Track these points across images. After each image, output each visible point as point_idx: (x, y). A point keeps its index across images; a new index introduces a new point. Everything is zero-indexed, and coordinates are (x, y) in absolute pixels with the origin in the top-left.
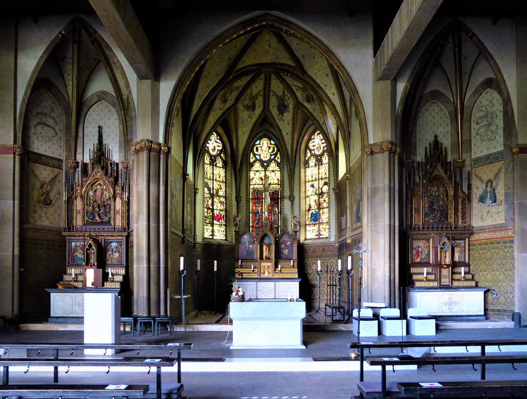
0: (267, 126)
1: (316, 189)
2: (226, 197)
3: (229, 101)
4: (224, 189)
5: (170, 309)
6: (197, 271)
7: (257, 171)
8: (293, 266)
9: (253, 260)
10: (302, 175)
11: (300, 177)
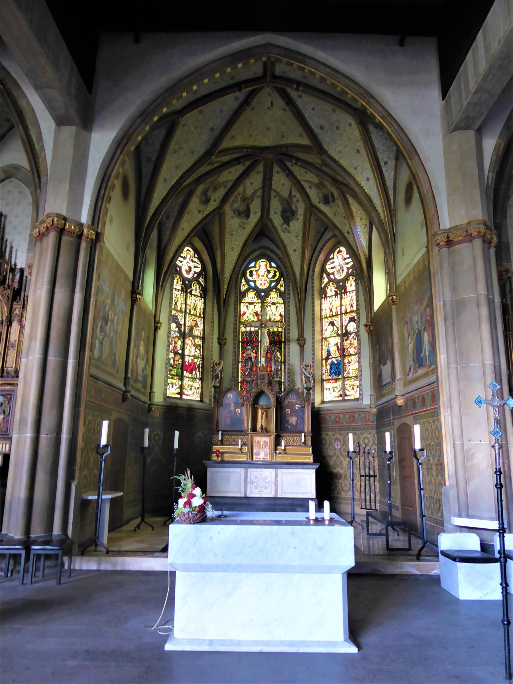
0: (265, 242)
1: (338, 328)
2: (203, 339)
3: (212, 202)
4: (201, 327)
5: (73, 522)
6: (143, 449)
7: (251, 303)
8: (305, 443)
9: (241, 433)
10: (317, 308)
11: (313, 311)
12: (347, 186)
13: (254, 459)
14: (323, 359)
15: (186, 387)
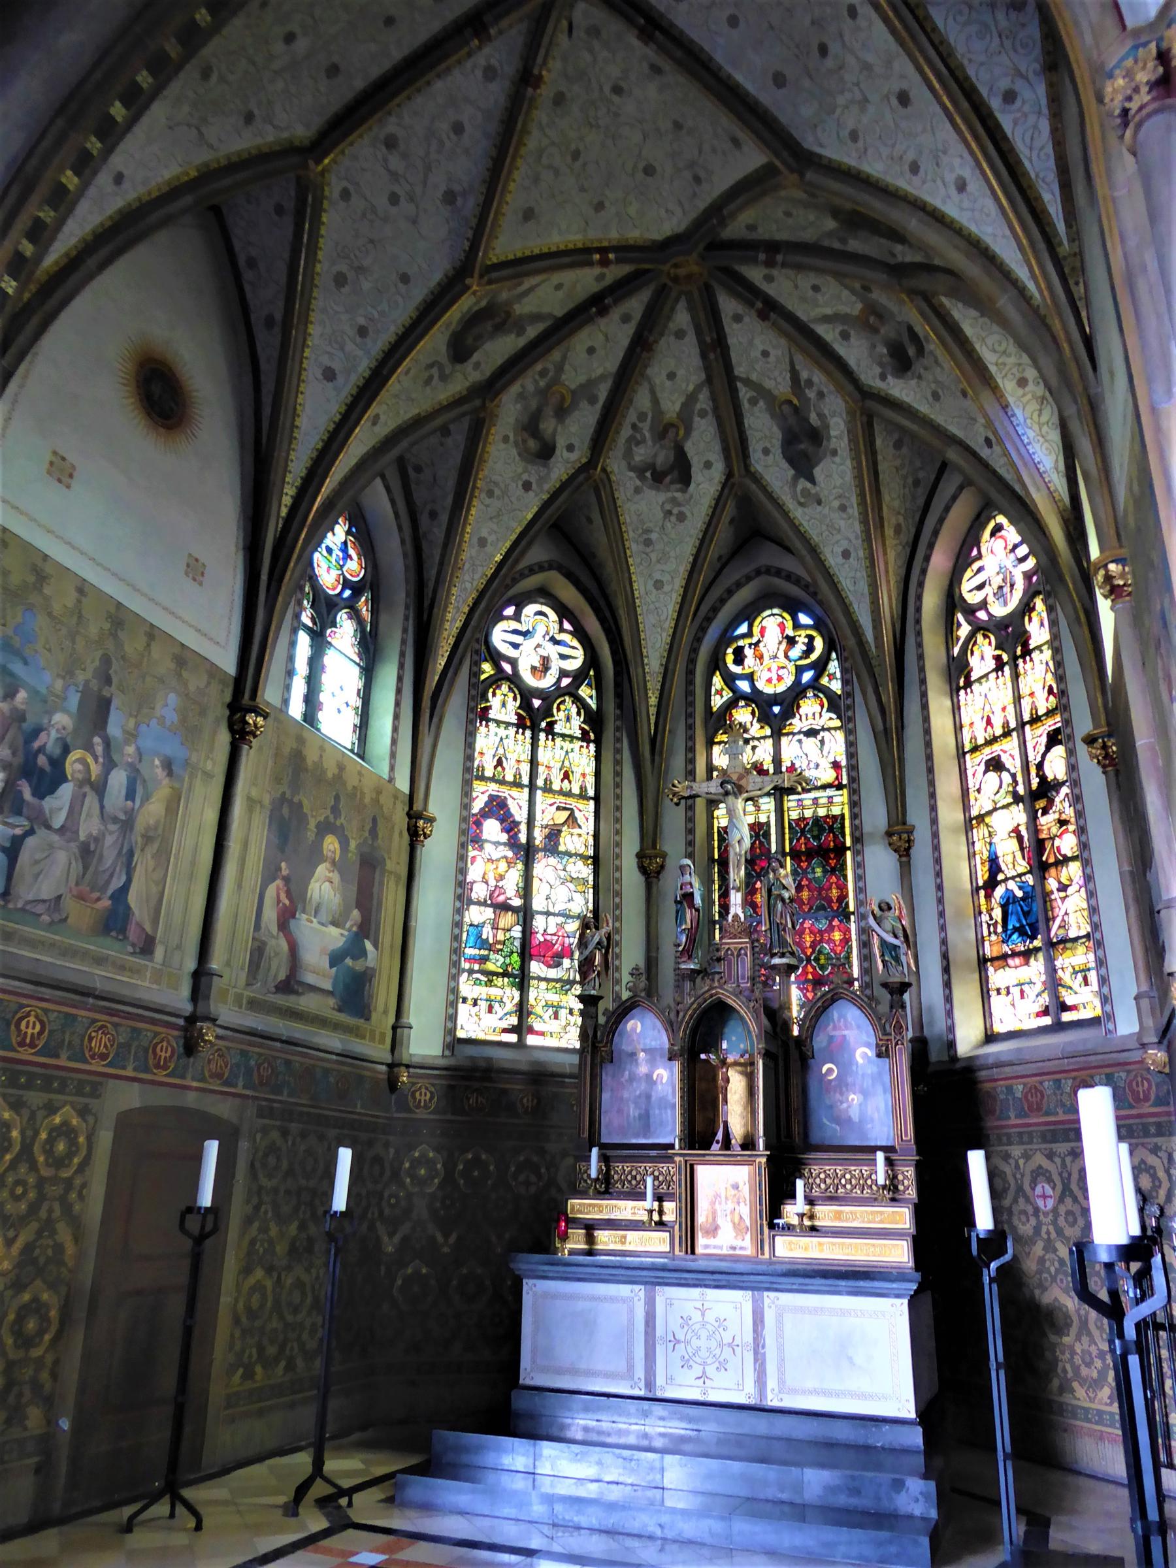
0: (769, 556)
1: (1014, 776)
2: (596, 860)
3: (561, 452)
4: (589, 827)
6: (192, 1209)
10: (941, 722)
12: (928, 268)
13: (699, 1250)
14: (978, 888)
15: (538, 1010)
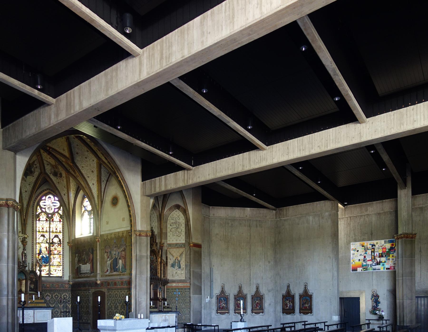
1: (47, 239)
